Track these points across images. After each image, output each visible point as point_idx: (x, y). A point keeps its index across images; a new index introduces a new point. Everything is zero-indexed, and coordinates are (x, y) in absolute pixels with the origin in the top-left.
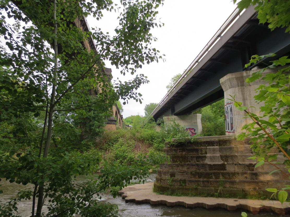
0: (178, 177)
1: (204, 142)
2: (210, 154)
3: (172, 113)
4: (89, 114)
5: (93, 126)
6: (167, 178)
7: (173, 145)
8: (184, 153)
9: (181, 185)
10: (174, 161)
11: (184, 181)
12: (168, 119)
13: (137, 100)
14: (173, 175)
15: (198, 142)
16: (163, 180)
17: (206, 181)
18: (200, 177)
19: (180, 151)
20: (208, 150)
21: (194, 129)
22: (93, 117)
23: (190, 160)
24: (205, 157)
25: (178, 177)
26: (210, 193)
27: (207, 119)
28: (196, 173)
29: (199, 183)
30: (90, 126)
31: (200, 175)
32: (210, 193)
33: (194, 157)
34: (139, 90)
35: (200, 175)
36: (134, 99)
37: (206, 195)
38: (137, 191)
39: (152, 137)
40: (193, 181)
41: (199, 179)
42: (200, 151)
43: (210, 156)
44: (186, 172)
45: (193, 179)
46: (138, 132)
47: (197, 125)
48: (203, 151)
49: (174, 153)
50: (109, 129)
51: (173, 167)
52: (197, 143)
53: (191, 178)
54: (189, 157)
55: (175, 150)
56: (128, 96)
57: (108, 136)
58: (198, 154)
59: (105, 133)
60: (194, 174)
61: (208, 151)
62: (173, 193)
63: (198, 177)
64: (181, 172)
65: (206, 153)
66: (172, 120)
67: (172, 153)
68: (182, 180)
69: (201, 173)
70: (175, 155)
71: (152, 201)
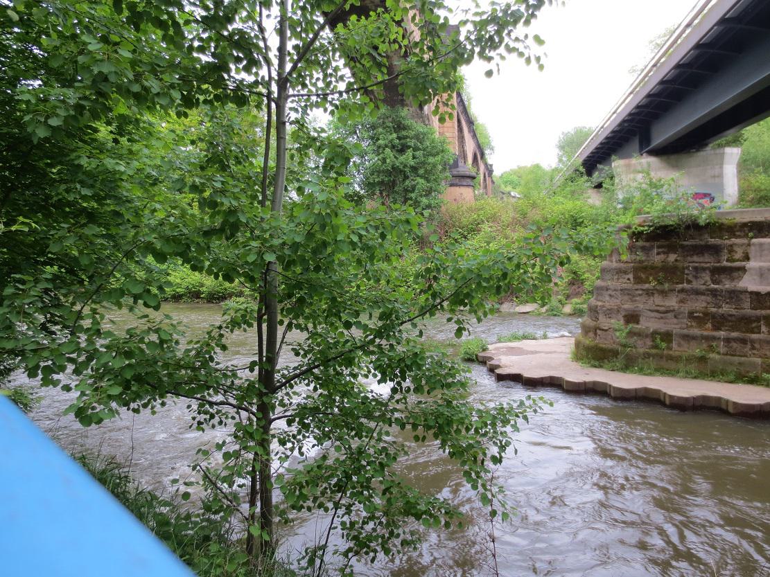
0: (649, 324)
1: (744, 225)
2: (762, 261)
3: (641, 149)
4: (402, 158)
5: (413, 190)
6: (616, 327)
7: (637, 236)
8: (672, 257)
9: (656, 347)
10: (638, 280)
11: (667, 337)
12: (628, 166)
13: (528, 60)
14: (632, 318)
15: (722, 224)
16: (603, 330)
17: (735, 340)
18: (717, 328)
19: (660, 250)
20: (752, 248)
21: (710, 195)
22: (412, 167)
23: (690, 278)
24: (743, 269)
25: (649, 324)
26: (748, 372)
27: (758, 166)
28: (706, 314)
29: (714, 344)
30: (406, 191)
31: (719, 322)
32: (748, 372)
33: (704, 269)
34: (536, 27)
35: (719, 322)
36: (521, 54)
37: (732, 377)
38: (529, 356)
39: (575, 220)
40: (694, 338)
41: (716, 334)
42: (726, 251)
43: (761, 268)
44: (673, 311)
45: (696, 331)
46: (534, 205)
47: (722, 183)
48: (736, 252)
49: (641, 256)
50: (455, 200)
51: (634, 296)
52: (717, 228)
53: (688, 327)
54: (687, 268)
55: (643, 248)
56: (502, 50)
57: (451, 217)
58: (719, 262)
59: (443, 209)
60: (699, 319)
61: (752, 252)
62: (628, 365)
63: (713, 325)
64: (657, 311)
65: (747, 258)
66: (640, 169)
67: (633, 257)
68: (659, 334)
69: (723, 315)
70: (643, 262)
71: (568, 382)
